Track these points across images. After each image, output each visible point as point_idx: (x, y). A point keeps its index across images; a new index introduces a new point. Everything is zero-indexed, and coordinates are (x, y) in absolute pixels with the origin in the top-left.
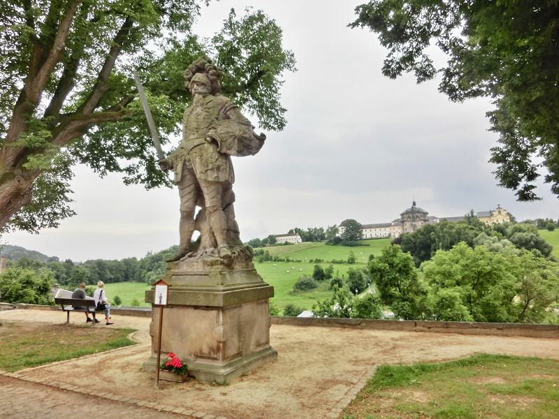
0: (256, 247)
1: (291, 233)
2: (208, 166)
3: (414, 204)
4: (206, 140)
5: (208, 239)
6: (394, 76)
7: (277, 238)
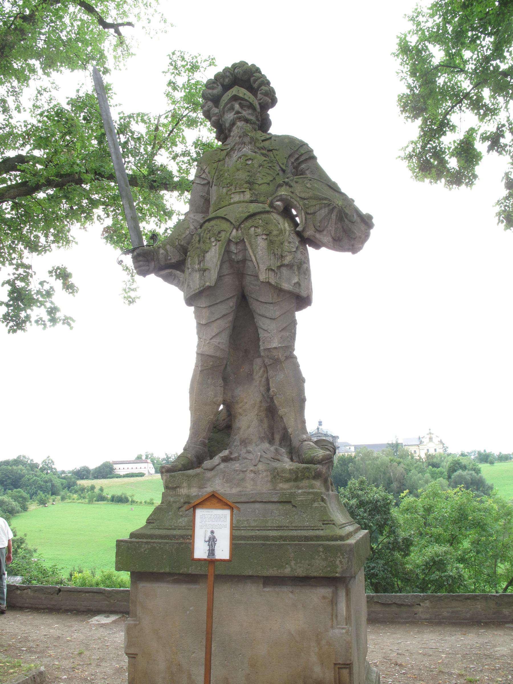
0: (82, 479)
1: (139, 459)
3: (320, 423)
4: (271, 205)
5: (255, 422)
6: (122, 112)
7: (115, 466)
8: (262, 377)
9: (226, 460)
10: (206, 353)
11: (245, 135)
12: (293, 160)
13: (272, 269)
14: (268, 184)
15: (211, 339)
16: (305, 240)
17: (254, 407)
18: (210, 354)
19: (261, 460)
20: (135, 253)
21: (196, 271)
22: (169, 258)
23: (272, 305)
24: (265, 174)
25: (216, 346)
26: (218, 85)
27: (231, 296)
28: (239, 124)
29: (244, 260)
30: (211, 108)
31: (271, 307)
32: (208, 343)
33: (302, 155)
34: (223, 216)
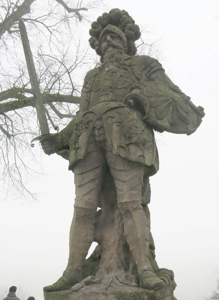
2: (130, 138)
5: (115, 255)
8: (120, 222)
9: (88, 283)
10: (79, 206)
11: (113, 56)
12: (146, 72)
13: (122, 147)
14: (126, 88)
15: (83, 196)
16: (153, 127)
17: (115, 244)
18: (81, 206)
19: (111, 285)
20: (42, 139)
21: (73, 149)
22: (64, 142)
23: (123, 172)
24: (123, 81)
25: (87, 201)
26: (99, 25)
27: (97, 166)
28: (110, 49)
29: (105, 141)
30: (95, 41)
31: (123, 173)
32: (81, 199)
33: (152, 68)
34: (92, 111)
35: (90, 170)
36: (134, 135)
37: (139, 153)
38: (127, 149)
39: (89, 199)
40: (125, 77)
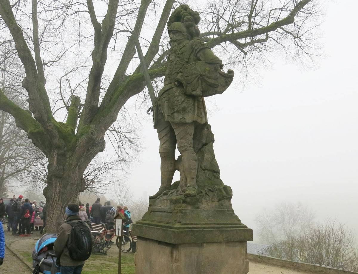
2: (174, 109)
13: (169, 116)
33: (196, 50)
35: (163, 130)
36: (176, 107)
37: (181, 117)
38: (172, 116)
39: (165, 147)
40: (178, 64)
